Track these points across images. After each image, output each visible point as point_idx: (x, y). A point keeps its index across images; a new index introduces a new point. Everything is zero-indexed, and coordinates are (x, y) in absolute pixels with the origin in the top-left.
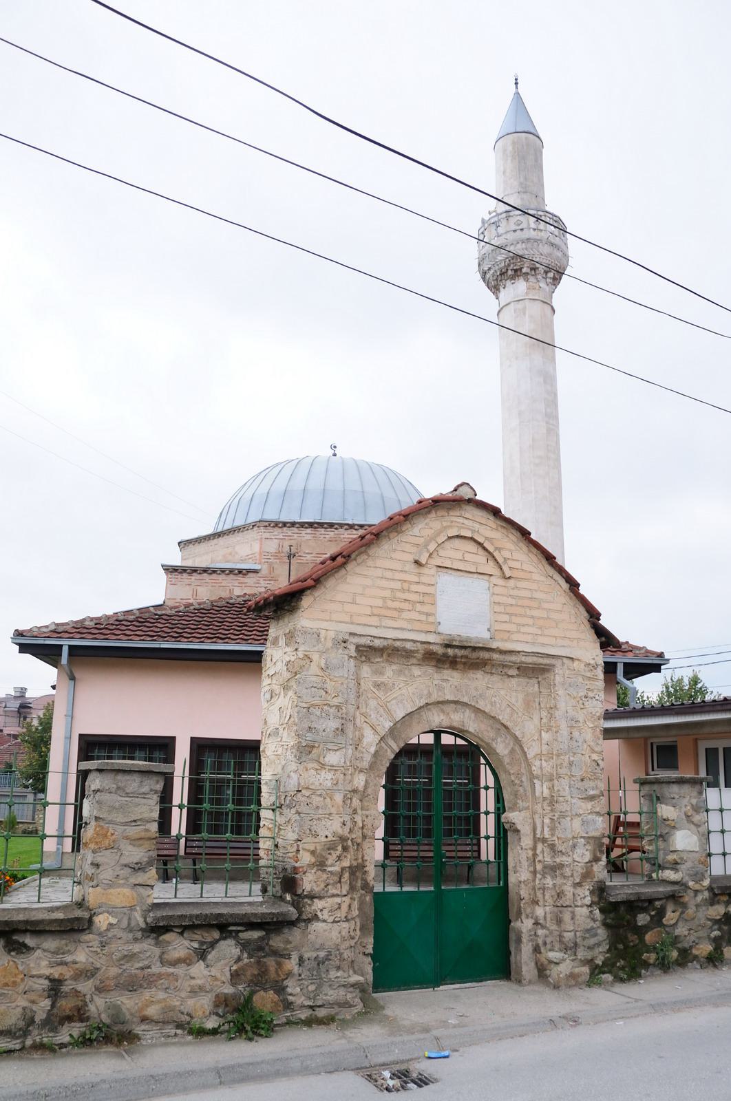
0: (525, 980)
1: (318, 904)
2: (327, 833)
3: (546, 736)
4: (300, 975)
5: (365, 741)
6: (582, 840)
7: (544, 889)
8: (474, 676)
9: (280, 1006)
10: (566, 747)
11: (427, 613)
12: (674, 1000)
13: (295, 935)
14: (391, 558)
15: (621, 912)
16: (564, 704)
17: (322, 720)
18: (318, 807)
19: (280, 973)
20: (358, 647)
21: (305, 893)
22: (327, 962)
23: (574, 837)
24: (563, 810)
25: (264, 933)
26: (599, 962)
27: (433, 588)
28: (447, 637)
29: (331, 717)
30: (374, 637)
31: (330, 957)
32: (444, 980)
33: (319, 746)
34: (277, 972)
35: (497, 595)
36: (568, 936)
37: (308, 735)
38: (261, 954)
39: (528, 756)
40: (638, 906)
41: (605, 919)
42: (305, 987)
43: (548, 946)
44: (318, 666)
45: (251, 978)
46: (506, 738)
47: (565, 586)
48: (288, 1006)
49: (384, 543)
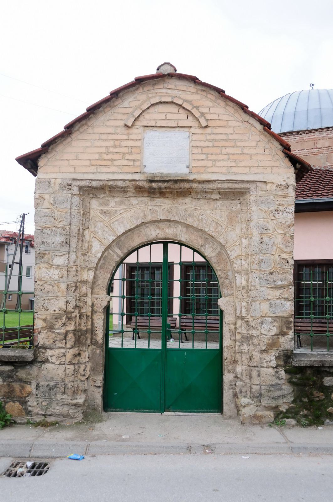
0: (226, 415)
1: (49, 353)
2: (55, 308)
3: (245, 242)
4: (37, 395)
5: (94, 250)
6: (270, 318)
7: (241, 353)
8: (184, 201)
9: (23, 412)
10: (257, 249)
11: (134, 160)
12: (317, 446)
13: (34, 370)
14: (106, 126)
15: (307, 374)
16: (256, 217)
17: (51, 237)
18: (48, 292)
19: (23, 392)
20: (80, 188)
21: (39, 345)
22: (55, 389)
23: (262, 316)
24: (254, 296)
25: (13, 368)
26: (284, 408)
27: (140, 142)
28: (150, 175)
29: (58, 235)
30: (92, 180)
31: (57, 386)
32: (168, 409)
33: (49, 253)
34: (21, 391)
35: (195, 140)
36: (255, 388)
37: (41, 246)
38: (10, 380)
39: (231, 257)
40: (326, 371)
41: (291, 378)
42: (40, 402)
43: (243, 394)
44: (49, 202)
45: (4, 394)
46: (214, 244)
47: (260, 127)
48: (29, 413)
49: (100, 116)
